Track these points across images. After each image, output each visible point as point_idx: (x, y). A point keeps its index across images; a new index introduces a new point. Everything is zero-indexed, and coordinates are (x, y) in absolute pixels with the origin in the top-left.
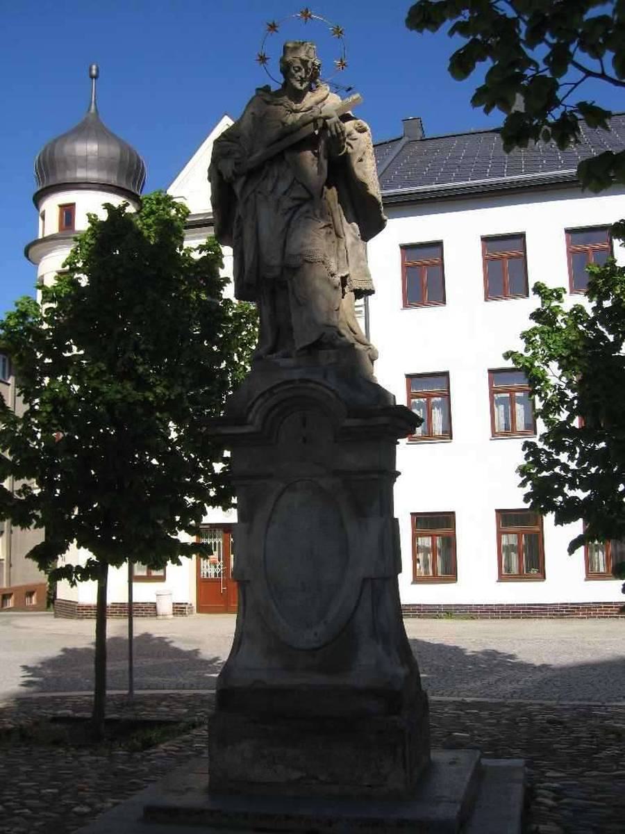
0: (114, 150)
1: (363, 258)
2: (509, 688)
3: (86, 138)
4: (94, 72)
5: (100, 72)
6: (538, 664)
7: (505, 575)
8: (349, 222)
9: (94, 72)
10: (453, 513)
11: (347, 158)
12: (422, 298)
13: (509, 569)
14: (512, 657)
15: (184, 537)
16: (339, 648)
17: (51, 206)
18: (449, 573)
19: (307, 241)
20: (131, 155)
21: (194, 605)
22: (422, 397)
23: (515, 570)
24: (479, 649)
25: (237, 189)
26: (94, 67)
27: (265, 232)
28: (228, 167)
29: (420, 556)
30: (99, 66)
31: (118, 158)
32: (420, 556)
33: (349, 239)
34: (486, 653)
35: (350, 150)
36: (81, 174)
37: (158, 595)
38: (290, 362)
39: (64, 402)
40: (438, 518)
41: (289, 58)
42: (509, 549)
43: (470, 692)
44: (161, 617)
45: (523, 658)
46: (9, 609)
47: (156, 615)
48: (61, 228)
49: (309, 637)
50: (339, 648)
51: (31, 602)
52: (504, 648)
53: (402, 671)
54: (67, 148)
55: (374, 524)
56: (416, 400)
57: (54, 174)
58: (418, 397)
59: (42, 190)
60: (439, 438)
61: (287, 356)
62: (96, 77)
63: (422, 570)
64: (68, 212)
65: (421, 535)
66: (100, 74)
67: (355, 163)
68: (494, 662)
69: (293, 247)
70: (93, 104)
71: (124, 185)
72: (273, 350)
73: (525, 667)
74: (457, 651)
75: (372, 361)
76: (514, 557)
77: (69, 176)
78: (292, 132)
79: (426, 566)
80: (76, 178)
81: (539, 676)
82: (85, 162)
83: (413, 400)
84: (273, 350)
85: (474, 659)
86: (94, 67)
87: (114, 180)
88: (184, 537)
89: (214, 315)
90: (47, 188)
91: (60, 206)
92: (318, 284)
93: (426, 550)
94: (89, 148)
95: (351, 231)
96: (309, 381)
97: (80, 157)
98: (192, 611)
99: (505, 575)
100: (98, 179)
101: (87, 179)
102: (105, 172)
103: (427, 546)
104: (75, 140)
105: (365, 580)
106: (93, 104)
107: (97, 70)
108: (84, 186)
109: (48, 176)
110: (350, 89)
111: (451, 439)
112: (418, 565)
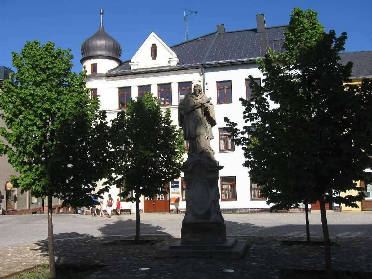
0: (111, 43)
1: (211, 132)
2: (251, 232)
3: (100, 39)
4: (102, 12)
5: (104, 11)
6: (261, 226)
7: (253, 198)
8: (208, 124)
9: (102, 12)
10: (235, 177)
11: (208, 112)
12: (224, 99)
13: (254, 196)
14: (253, 224)
15: (160, 189)
16: (208, 214)
17: (88, 64)
18: (234, 198)
19: (200, 130)
20: (117, 45)
21: (143, 210)
22: (225, 136)
23: (257, 197)
24: (242, 222)
25: (185, 117)
26: (102, 10)
27: (191, 127)
28: (183, 112)
29: (224, 192)
30: (104, 9)
31: (112, 47)
32: (224, 192)
33: (208, 128)
34: (244, 224)
35: (209, 110)
36: (99, 53)
37: (131, 206)
38: (197, 155)
39: (68, 125)
40: (229, 178)
41: (196, 89)
42: (254, 189)
43: (238, 233)
44: (132, 214)
45: (257, 225)
46: (61, 213)
47: (130, 213)
48: (92, 73)
49: (202, 213)
50: (208, 214)
51: (69, 210)
52: (251, 222)
53: (221, 219)
54: (94, 43)
55: (215, 190)
56: (222, 137)
57: (89, 53)
58: (223, 136)
59: (83, 59)
60: (230, 150)
61: (196, 154)
62: (102, 14)
63: (224, 197)
64: (94, 66)
65: (224, 184)
66: (104, 13)
67: (210, 113)
68: (247, 226)
69: (197, 131)
70: (102, 24)
71: (115, 57)
72: (192, 153)
73: (256, 227)
74: (236, 223)
75: (214, 154)
76: (256, 192)
77: (95, 53)
78: (196, 106)
79: (226, 195)
80: (97, 54)
81: (259, 230)
82: (100, 48)
83: (221, 137)
84: (192, 153)
85: (241, 225)
86: (102, 10)
87: (111, 55)
88: (160, 189)
89: (169, 131)
90: (85, 58)
91: (91, 64)
92: (203, 139)
93: (226, 190)
94: (101, 42)
95: (209, 126)
96: (201, 160)
97: (99, 46)
98: (143, 212)
99: (253, 198)
100: (105, 55)
101: (101, 54)
102: (108, 52)
103: (226, 188)
104: (97, 39)
105: (213, 201)
106: (102, 24)
107: (103, 11)
108: (100, 57)
109: (86, 52)
110: (196, 12)
111: (234, 150)
112: (223, 195)
